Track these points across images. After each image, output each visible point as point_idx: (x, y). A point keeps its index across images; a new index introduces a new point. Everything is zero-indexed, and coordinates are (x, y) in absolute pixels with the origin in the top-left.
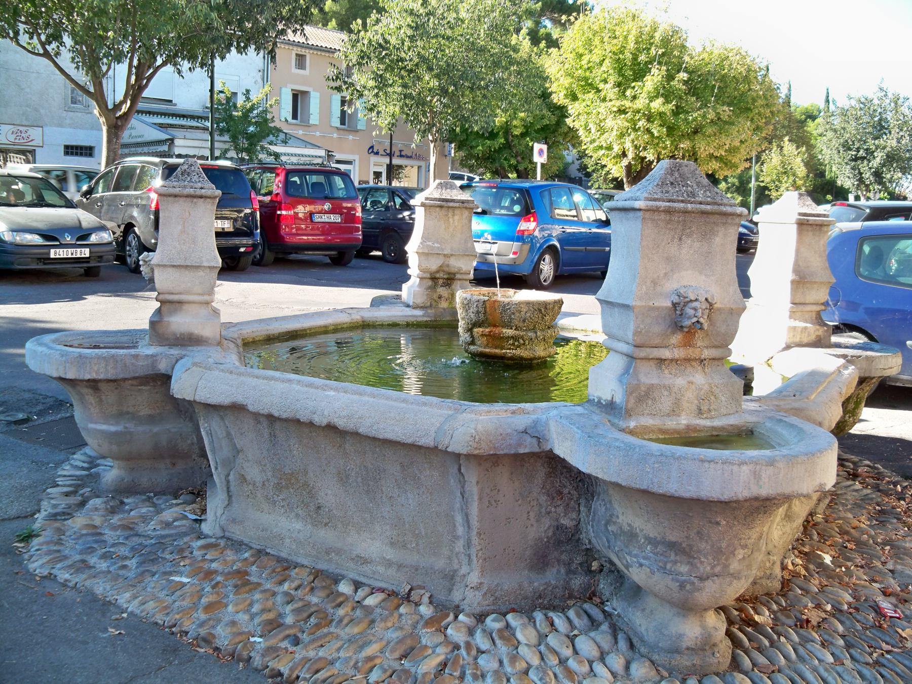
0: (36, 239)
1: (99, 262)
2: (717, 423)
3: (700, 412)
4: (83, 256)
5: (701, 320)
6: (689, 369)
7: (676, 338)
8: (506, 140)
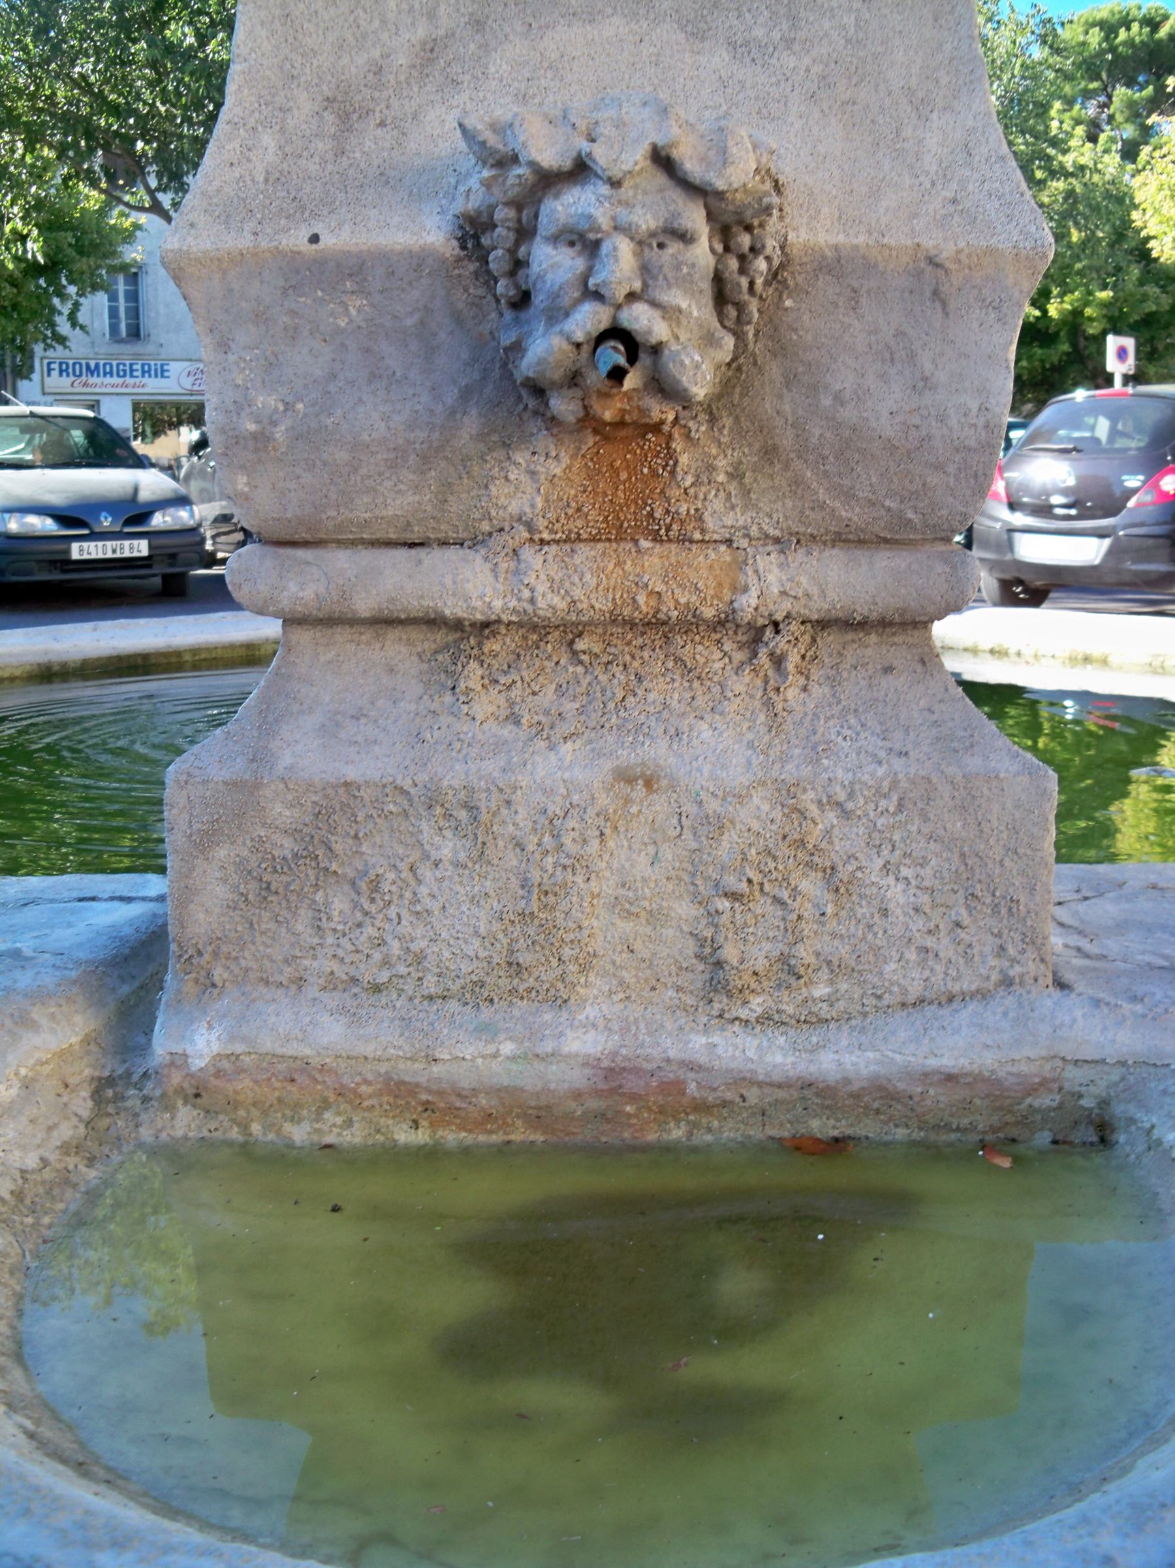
0: (45, 525)
1: (171, 565)
2: (843, 1059)
3: (716, 981)
4: (136, 554)
5: (642, 319)
6: (664, 689)
7: (535, 479)
8: (1074, 345)
